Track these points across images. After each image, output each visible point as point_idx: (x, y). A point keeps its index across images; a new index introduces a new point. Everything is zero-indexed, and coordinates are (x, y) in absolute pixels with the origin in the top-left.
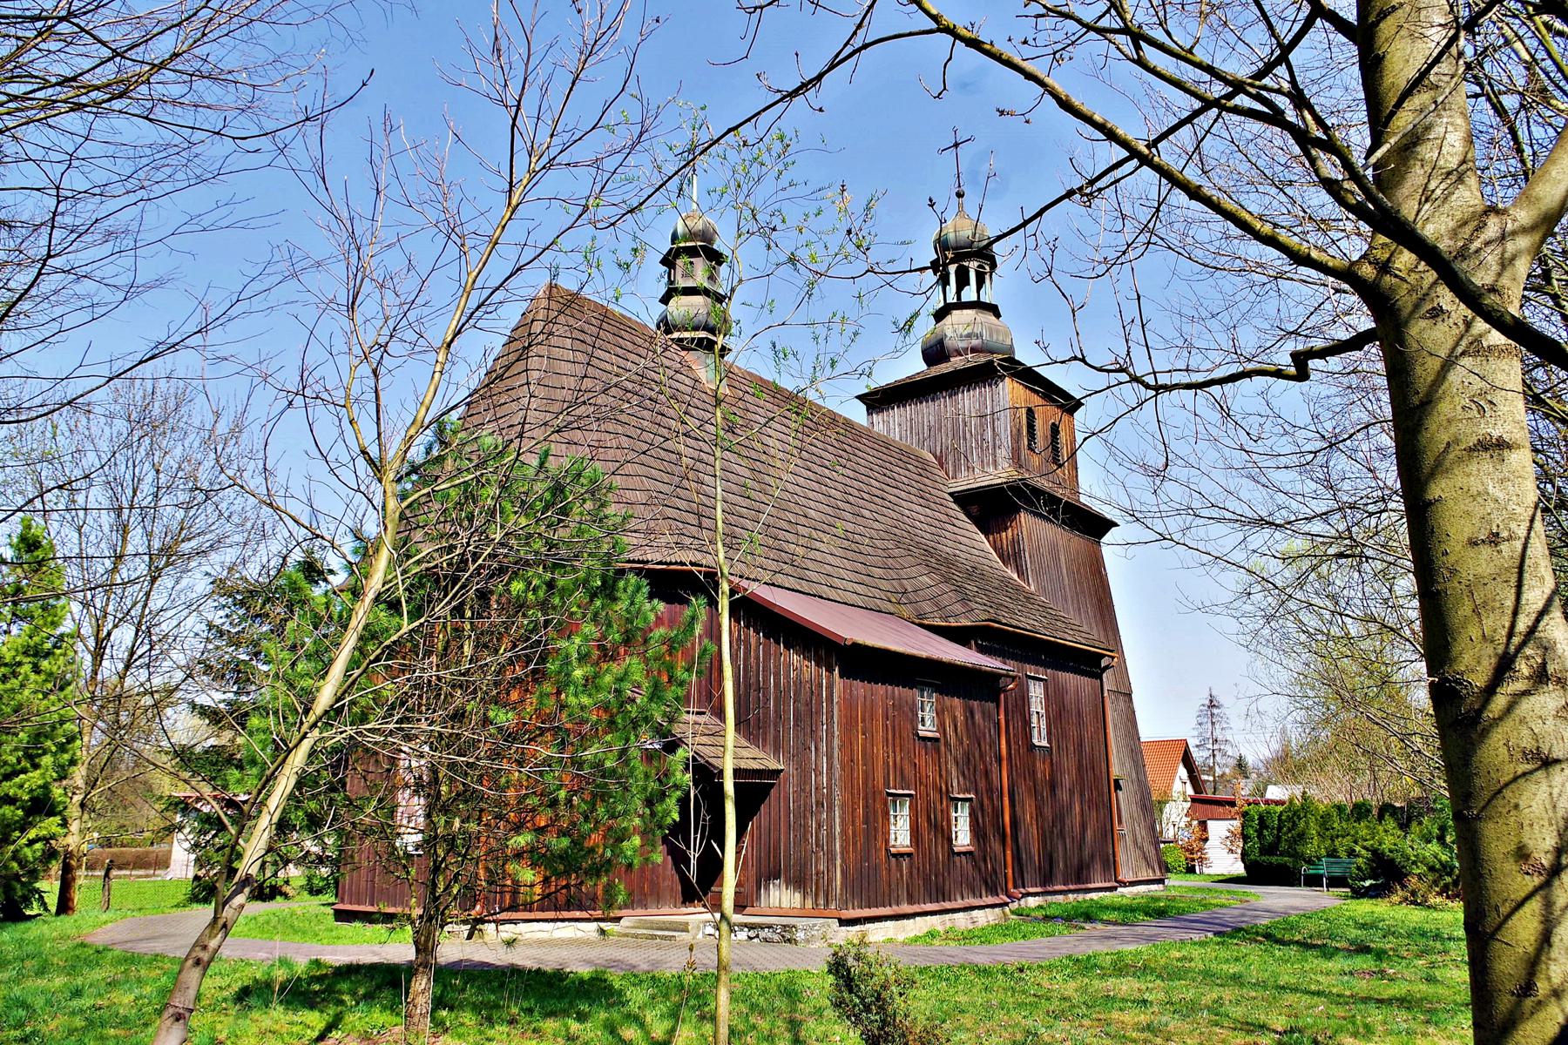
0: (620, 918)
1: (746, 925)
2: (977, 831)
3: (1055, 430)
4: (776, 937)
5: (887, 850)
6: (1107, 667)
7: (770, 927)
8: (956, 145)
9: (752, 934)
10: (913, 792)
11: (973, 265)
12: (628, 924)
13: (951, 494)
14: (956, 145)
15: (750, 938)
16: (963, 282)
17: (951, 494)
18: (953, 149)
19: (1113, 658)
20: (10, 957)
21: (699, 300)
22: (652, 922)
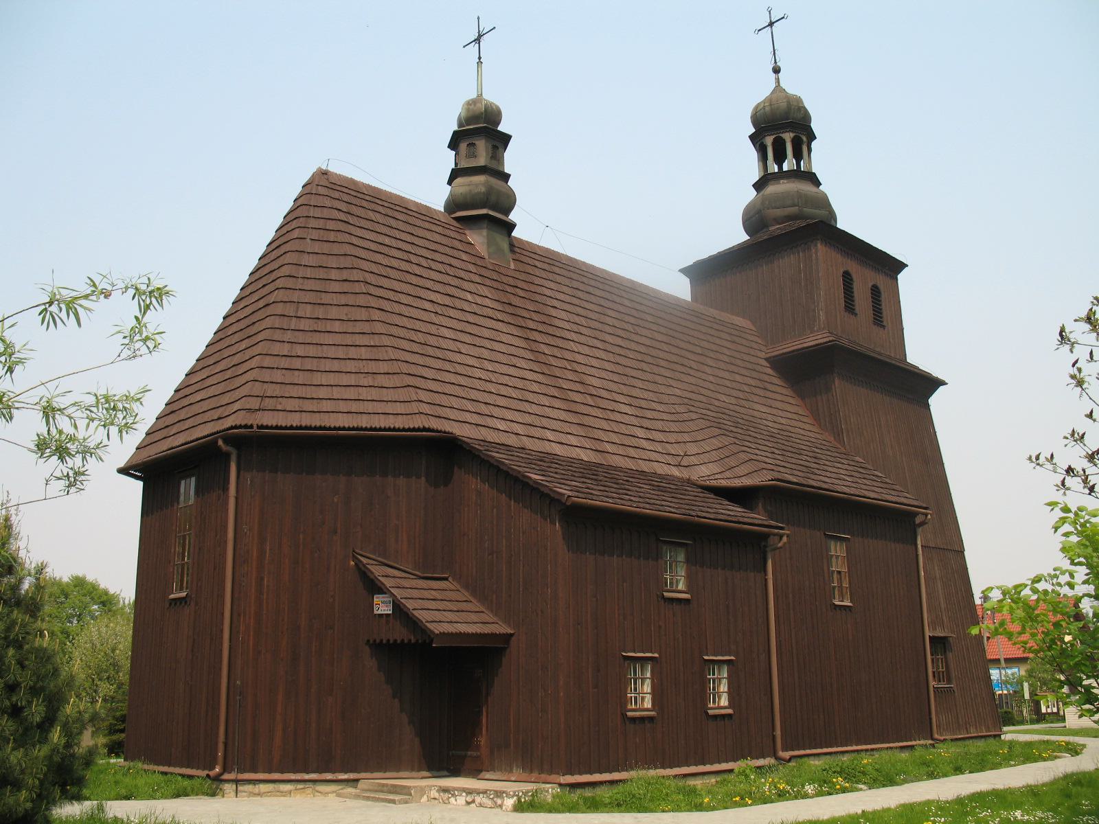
0: (357, 780)
1: (464, 790)
2: (657, 693)
3: (875, 291)
4: (489, 803)
5: (624, 715)
6: (923, 524)
7: (485, 792)
8: (771, 24)
9: (469, 799)
10: (656, 655)
11: (788, 137)
12: (366, 787)
13: (766, 359)
14: (771, 24)
15: (468, 803)
16: (780, 158)
17: (766, 359)
18: (769, 28)
19: (926, 515)
20: (29, 805)
21: (480, 179)
22: (384, 785)
